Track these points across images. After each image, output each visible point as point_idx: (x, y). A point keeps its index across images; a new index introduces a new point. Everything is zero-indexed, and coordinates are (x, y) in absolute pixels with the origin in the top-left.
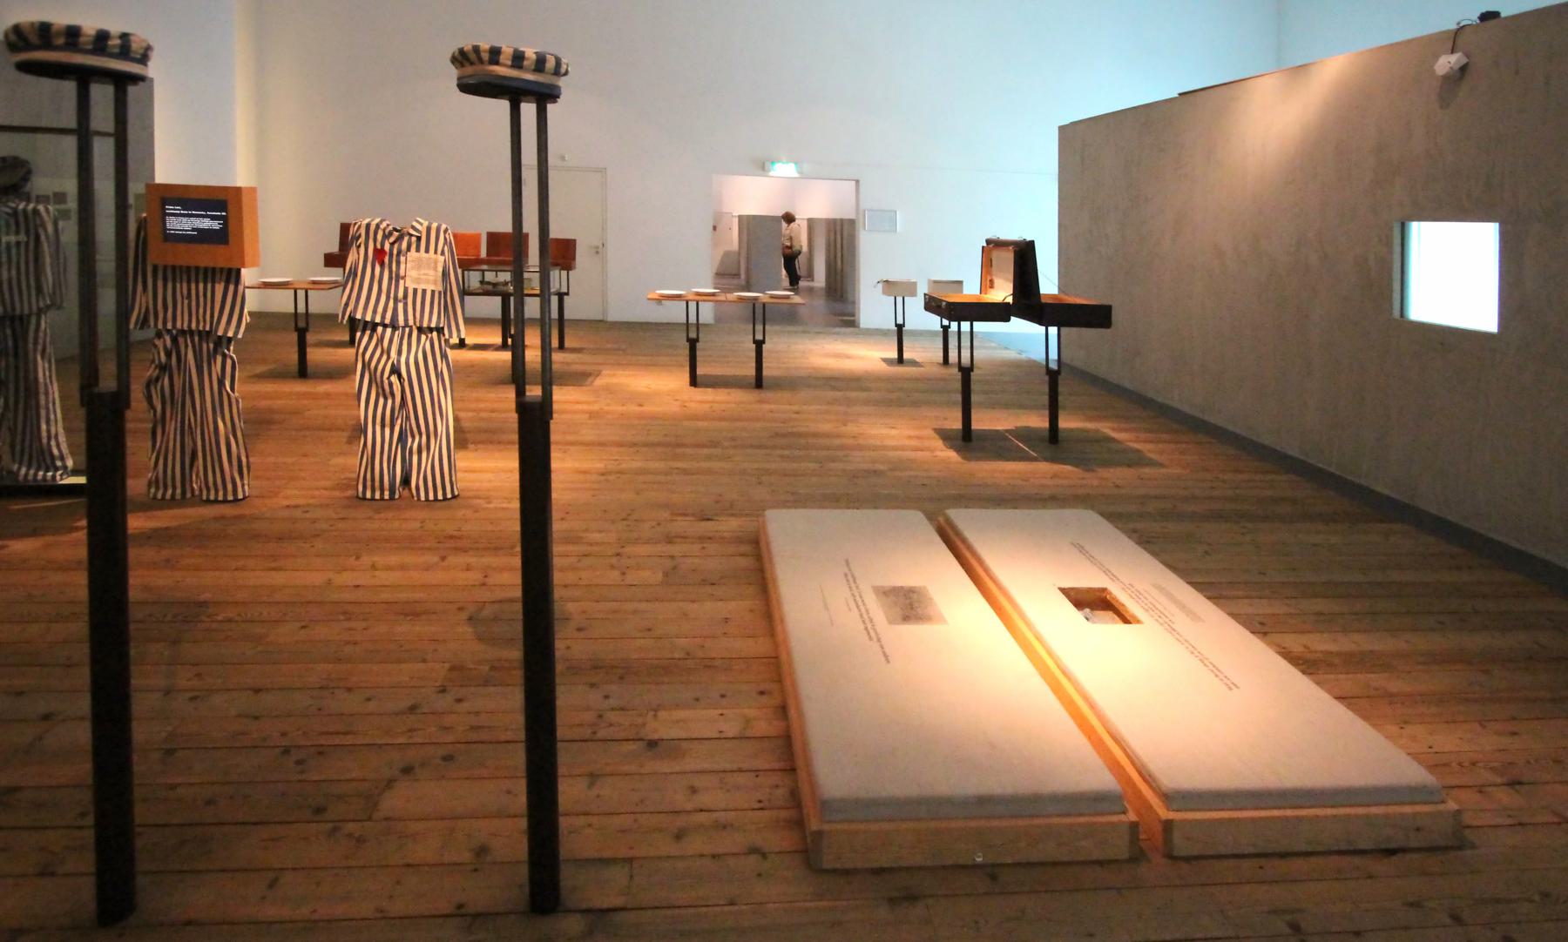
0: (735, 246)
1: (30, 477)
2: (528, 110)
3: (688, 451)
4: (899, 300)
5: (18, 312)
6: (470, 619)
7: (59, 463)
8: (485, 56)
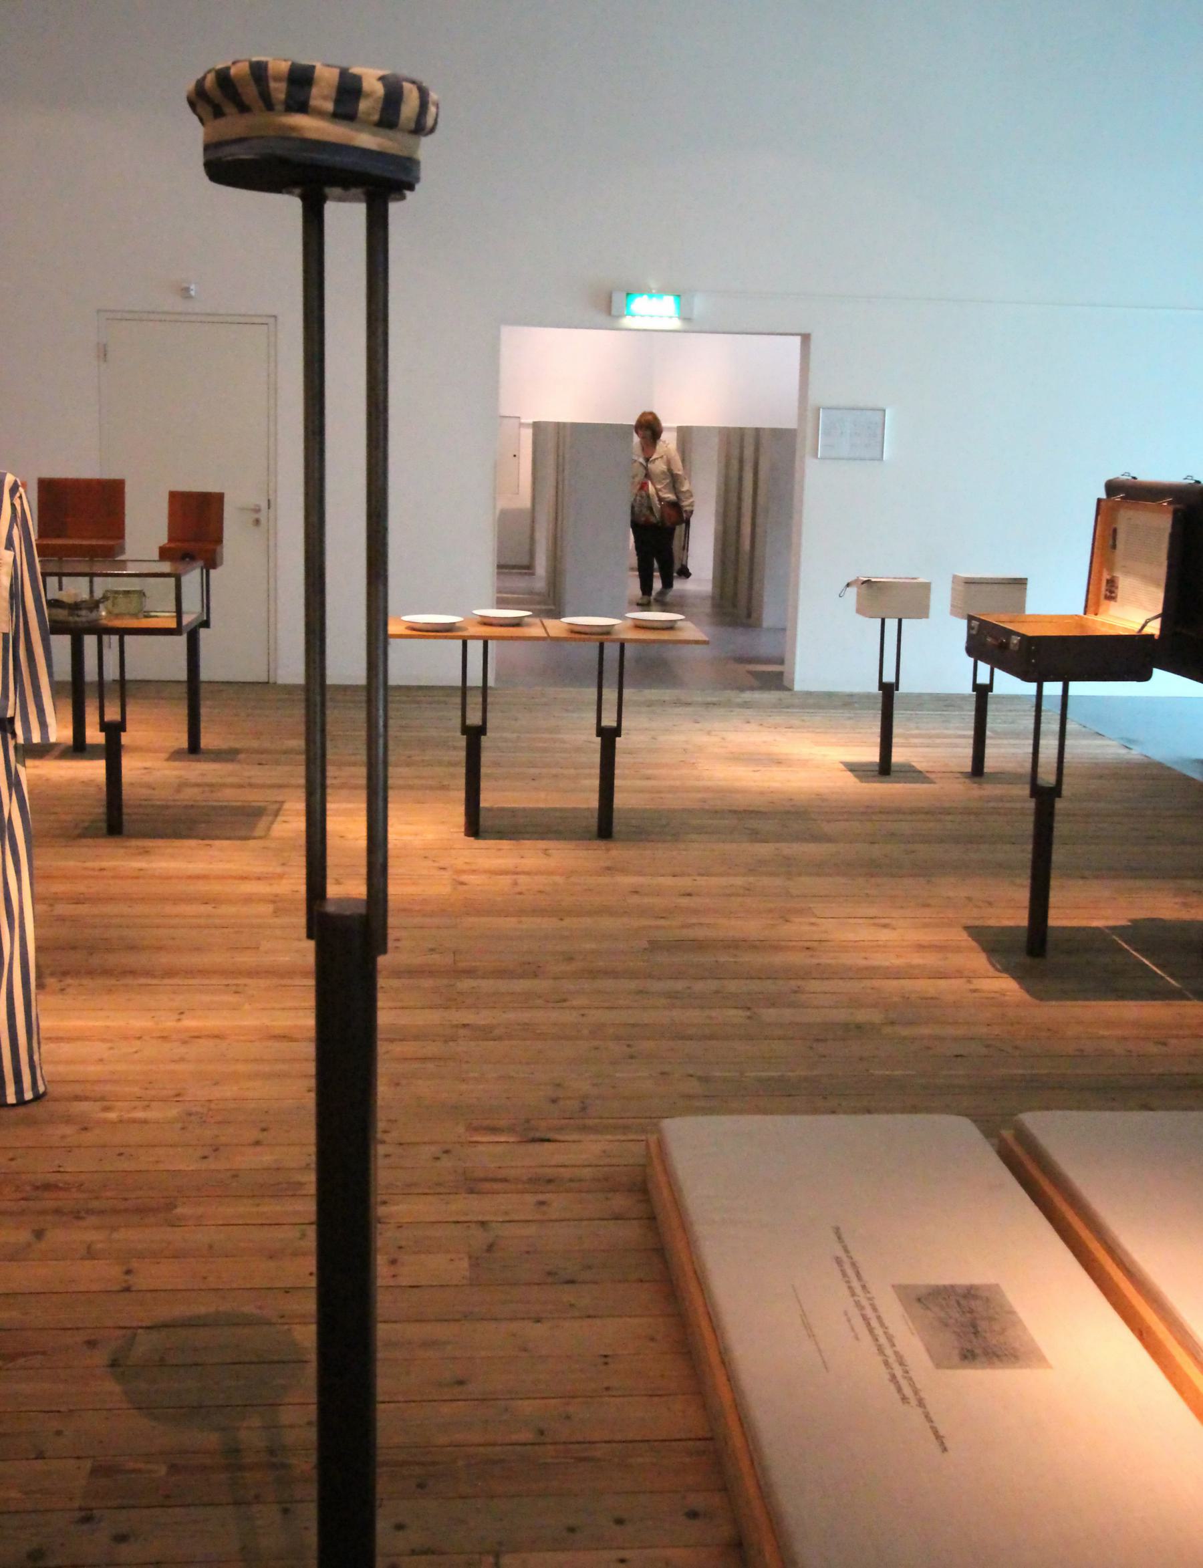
0: (524, 500)
2: (345, 219)
3: (487, 985)
4: (891, 624)
6: (114, 1364)
8: (279, 90)
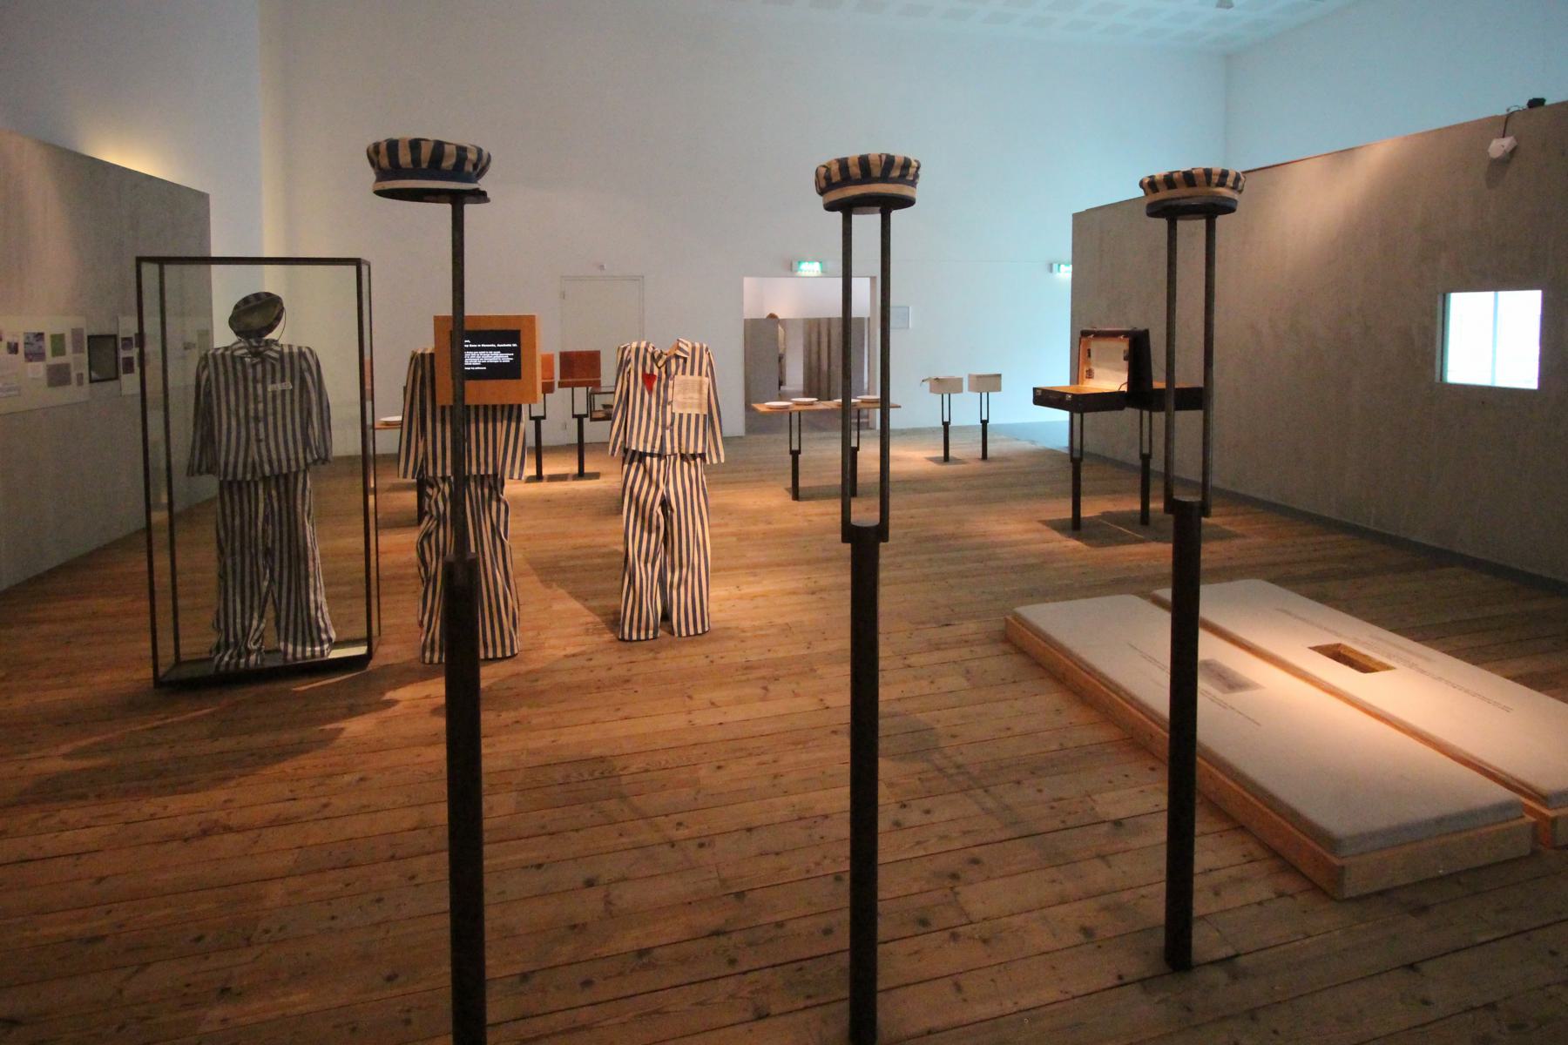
1: (308, 654)
5: (285, 471)
7: (324, 636)
